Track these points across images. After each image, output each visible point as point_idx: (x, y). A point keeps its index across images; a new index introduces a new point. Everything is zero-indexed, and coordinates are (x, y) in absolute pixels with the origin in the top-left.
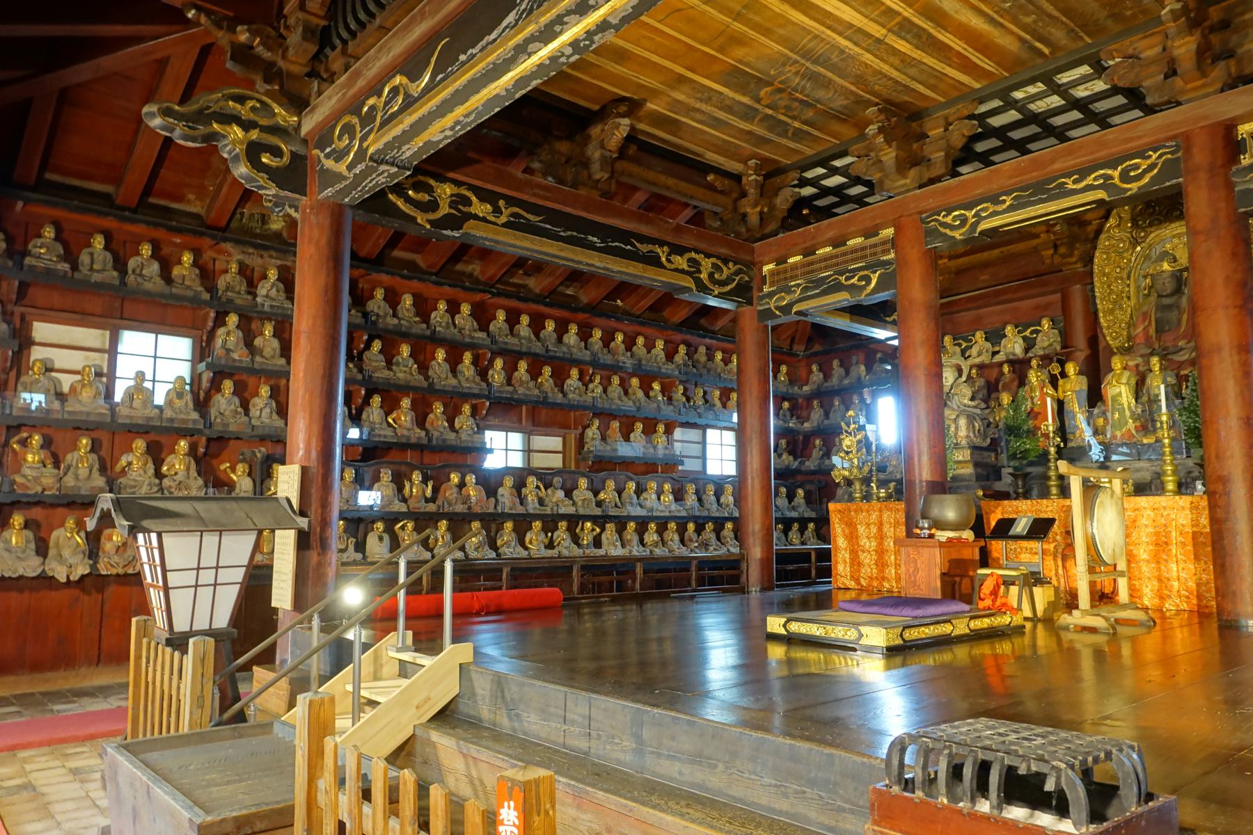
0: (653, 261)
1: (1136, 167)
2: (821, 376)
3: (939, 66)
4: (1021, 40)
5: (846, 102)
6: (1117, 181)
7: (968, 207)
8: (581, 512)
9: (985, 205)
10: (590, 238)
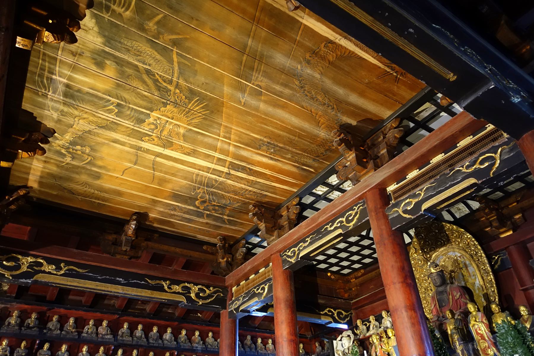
0: (161, 289)
1: (351, 215)
2: (320, 349)
3: (268, 183)
4: (298, 167)
6: (345, 223)
7: (295, 246)
10: (118, 279)
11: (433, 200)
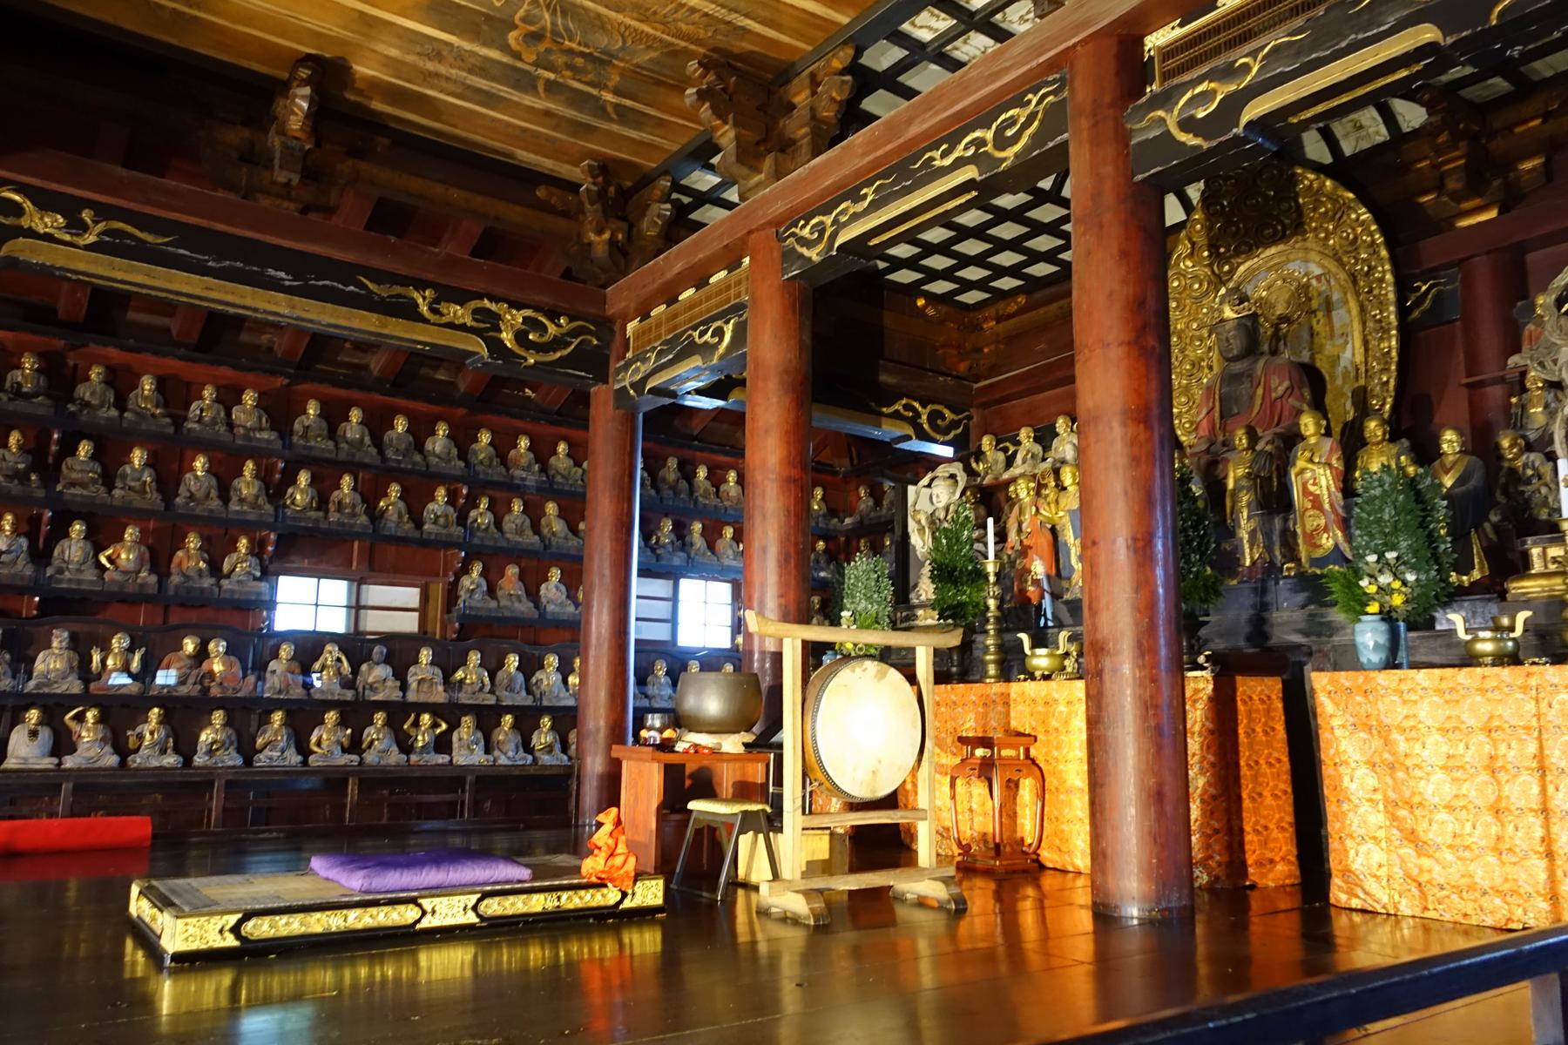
0: (408, 312)
1: (1012, 122)
2: (871, 503)
5: (654, 55)
6: (989, 148)
7: (826, 211)
8: (412, 697)
9: (843, 206)
10: (271, 272)
11: (1282, 93)
